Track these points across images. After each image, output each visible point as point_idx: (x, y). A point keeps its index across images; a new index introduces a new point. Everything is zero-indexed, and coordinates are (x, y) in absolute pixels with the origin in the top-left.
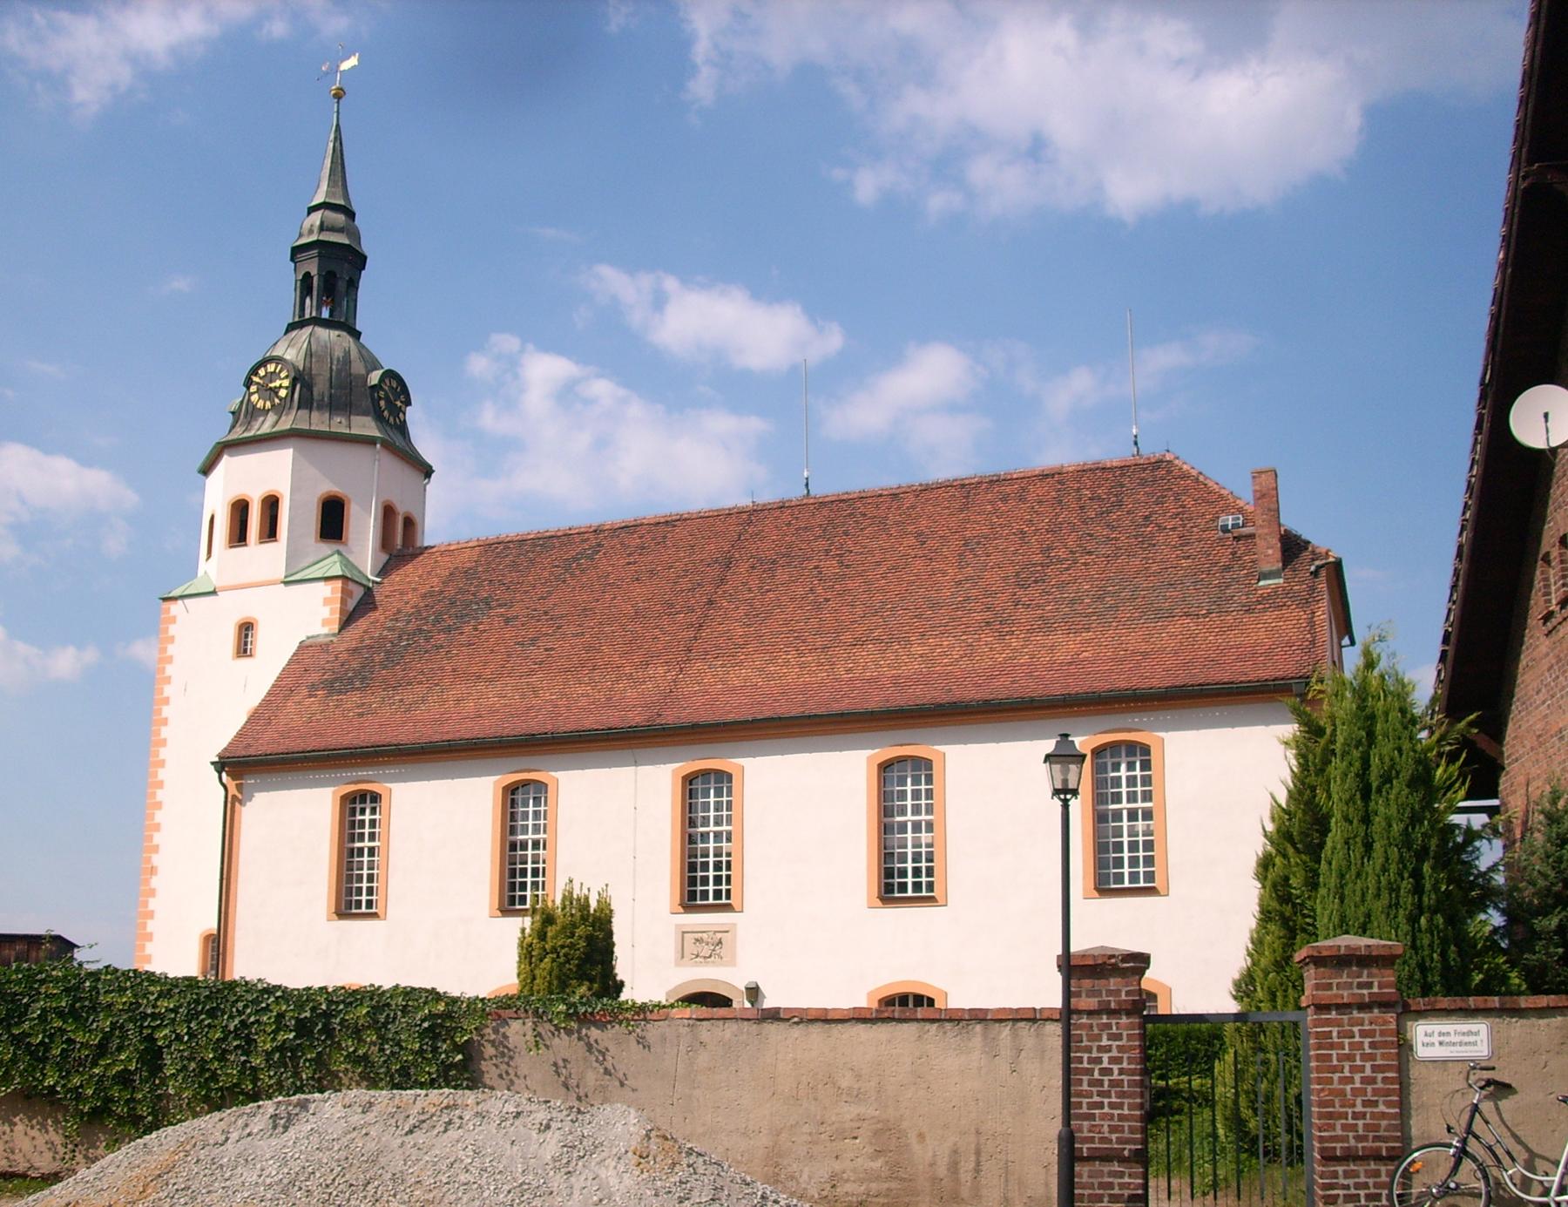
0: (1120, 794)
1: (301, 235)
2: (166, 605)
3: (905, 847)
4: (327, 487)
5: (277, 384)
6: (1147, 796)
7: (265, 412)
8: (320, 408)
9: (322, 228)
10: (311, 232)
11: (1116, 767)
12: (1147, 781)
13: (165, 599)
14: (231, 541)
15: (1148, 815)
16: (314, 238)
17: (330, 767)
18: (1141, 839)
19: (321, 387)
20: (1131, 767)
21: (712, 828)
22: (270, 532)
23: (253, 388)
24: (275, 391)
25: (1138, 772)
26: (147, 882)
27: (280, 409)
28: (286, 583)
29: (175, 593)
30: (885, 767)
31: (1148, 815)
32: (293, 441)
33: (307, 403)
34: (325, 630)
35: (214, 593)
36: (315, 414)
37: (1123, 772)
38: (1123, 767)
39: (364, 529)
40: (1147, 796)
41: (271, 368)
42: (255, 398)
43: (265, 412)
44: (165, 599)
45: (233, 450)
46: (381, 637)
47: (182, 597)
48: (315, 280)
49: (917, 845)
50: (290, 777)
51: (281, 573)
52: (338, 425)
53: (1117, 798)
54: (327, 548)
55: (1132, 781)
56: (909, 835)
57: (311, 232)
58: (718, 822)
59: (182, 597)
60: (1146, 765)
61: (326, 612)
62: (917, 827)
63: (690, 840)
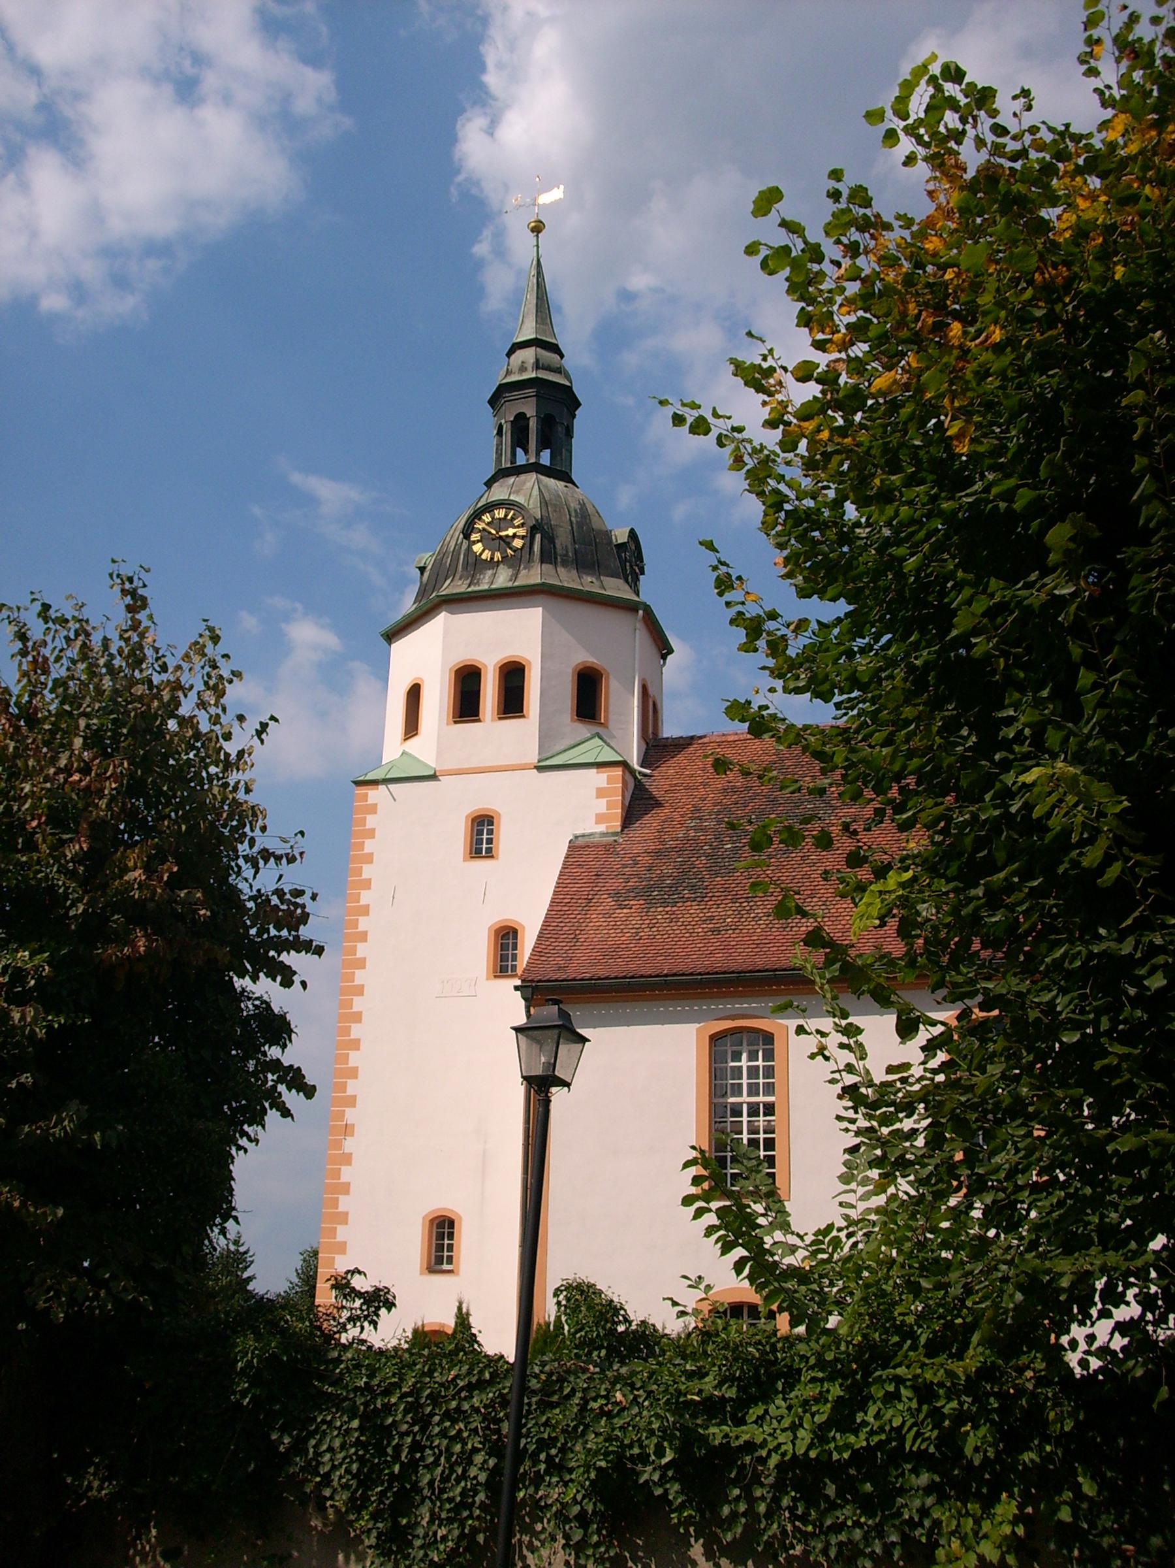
0: (740, 1085)
1: (508, 373)
2: (361, 791)
3: (741, 1133)
4: (582, 657)
5: (511, 532)
6: (769, 1089)
7: (492, 564)
8: (565, 564)
9: (538, 366)
10: (523, 369)
11: (737, 1056)
12: (769, 1072)
13: (358, 783)
14: (523, 716)
15: (770, 1109)
16: (531, 374)
17: (712, 996)
18: (762, 1136)
19: (563, 540)
20: (753, 1056)
21: (745, 1098)
22: (512, 703)
23: (475, 537)
24: (507, 541)
25: (760, 1063)
26: (338, 1145)
27: (515, 561)
28: (540, 769)
29: (369, 777)
30: (715, 1039)
31: (770, 1109)
32: (540, 598)
33: (549, 556)
34: (602, 828)
35: (433, 777)
36: (561, 570)
37: (744, 1063)
38: (744, 1056)
39: (624, 708)
40: (769, 1089)
41: (500, 513)
42: (478, 548)
43: (492, 564)
44: (358, 783)
45: (453, 606)
46: (687, 839)
47: (386, 781)
48: (533, 424)
49: (753, 1130)
50: (628, 1009)
51: (533, 757)
52: (588, 583)
53: (737, 1090)
54: (583, 730)
55: (753, 1072)
56: (745, 1119)
57: (523, 369)
58: (753, 1090)
59: (386, 781)
60: (769, 1055)
61: (601, 806)
62: (753, 1111)
63: (720, 1114)
